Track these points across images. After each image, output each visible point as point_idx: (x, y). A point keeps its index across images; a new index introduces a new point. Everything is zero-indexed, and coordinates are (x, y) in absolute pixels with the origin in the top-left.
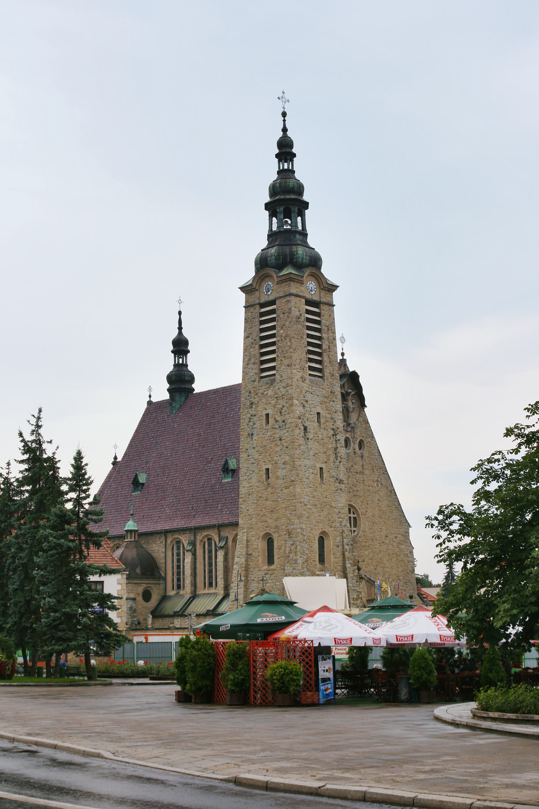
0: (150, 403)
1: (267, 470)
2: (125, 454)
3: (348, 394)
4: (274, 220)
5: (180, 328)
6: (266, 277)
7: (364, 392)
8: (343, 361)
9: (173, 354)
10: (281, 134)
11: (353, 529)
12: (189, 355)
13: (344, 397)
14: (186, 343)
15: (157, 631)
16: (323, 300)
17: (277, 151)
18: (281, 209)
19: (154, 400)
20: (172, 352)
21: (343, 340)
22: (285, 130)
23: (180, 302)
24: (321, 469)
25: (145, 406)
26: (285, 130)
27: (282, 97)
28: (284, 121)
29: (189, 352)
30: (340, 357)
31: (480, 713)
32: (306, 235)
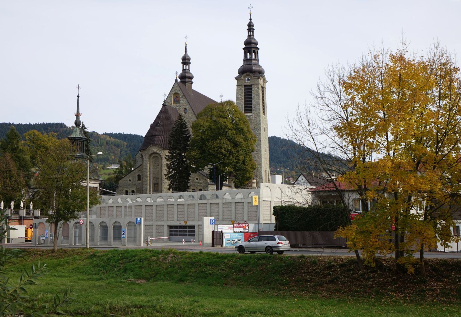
5: (186, 51)
9: (182, 64)
12: (190, 65)
20: (182, 63)
22: (251, 19)
26: (251, 19)
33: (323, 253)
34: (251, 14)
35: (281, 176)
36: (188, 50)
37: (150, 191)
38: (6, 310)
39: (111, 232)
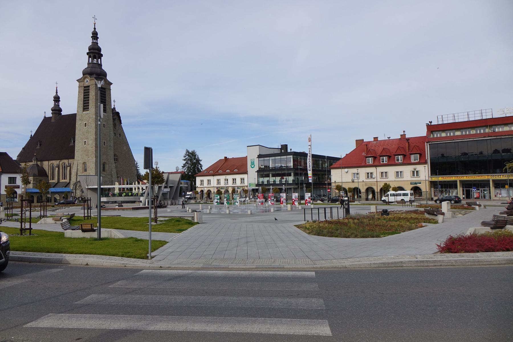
0: (45, 117)
1: (85, 141)
2: (34, 135)
3: (116, 119)
4: (90, 59)
5: (57, 93)
6: (86, 78)
7: (121, 119)
8: (114, 108)
9: (54, 101)
10: (93, 30)
11: (116, 162)
12: (60, 102)
13: (114, 120)
14: (59, 98)
15: (487, 150)
16: (107, 88)
17: (92, 35)
18: (92, 55)
19: (47, 116)
20: (54, 100)
21: (114, 101)
22: (95, 29)
23: (57, 83)
24: (104, 142)
25: (43, 118)
26: (95, 29)
27: (95, 19)
28: (95, 25)
29: (60, 101)
30: (112, 107)
31: (34, 255)
32: (102, 65)
33: (358, 261)
34: (95, 24)
35: (332, 170)
36: (58, 92)
37: (117, 188)
38: (32, 208)
39: (205, 196)
